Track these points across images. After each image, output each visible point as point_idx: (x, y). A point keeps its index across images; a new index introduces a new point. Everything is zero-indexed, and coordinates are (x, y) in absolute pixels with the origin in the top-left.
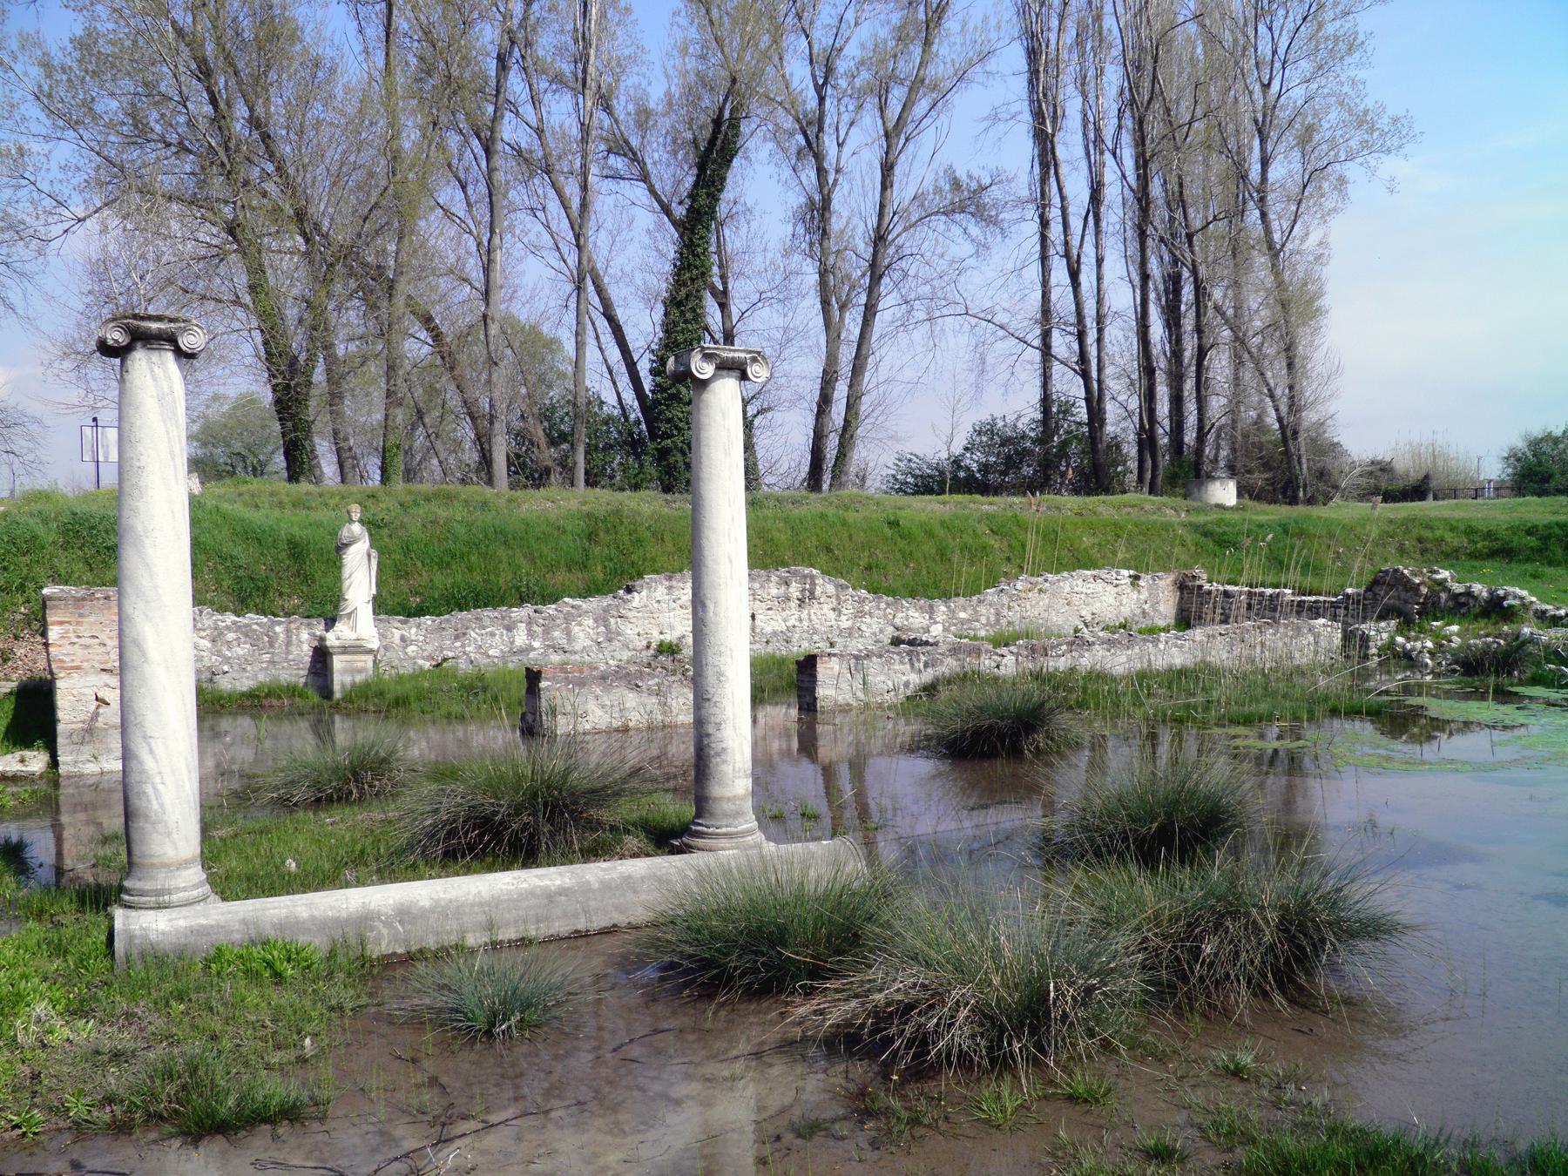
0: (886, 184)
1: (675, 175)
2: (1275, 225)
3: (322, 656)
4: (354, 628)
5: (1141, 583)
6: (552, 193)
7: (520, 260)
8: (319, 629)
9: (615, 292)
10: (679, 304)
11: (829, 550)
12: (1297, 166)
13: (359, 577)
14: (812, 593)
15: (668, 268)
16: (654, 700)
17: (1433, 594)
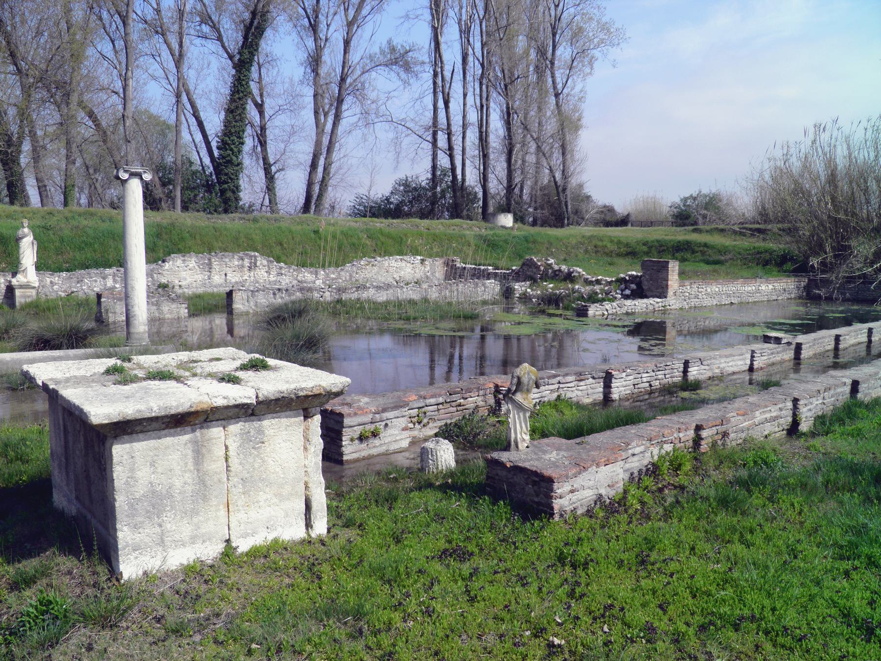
0: (346, 51)
1: (233, 37)
2: (558, 80)
4: (26, 277)
5: (426, 263)
6: (164, 47)
7: (145, 84)
8: (9, 278)
9: (200, 104)
10: (232, 112)
11: (281, 244)
12: (569, 50)
13: (28, 254)
14: (255, 264)
15: (228, 92)
16: (155, 308)
17: (546, 270)
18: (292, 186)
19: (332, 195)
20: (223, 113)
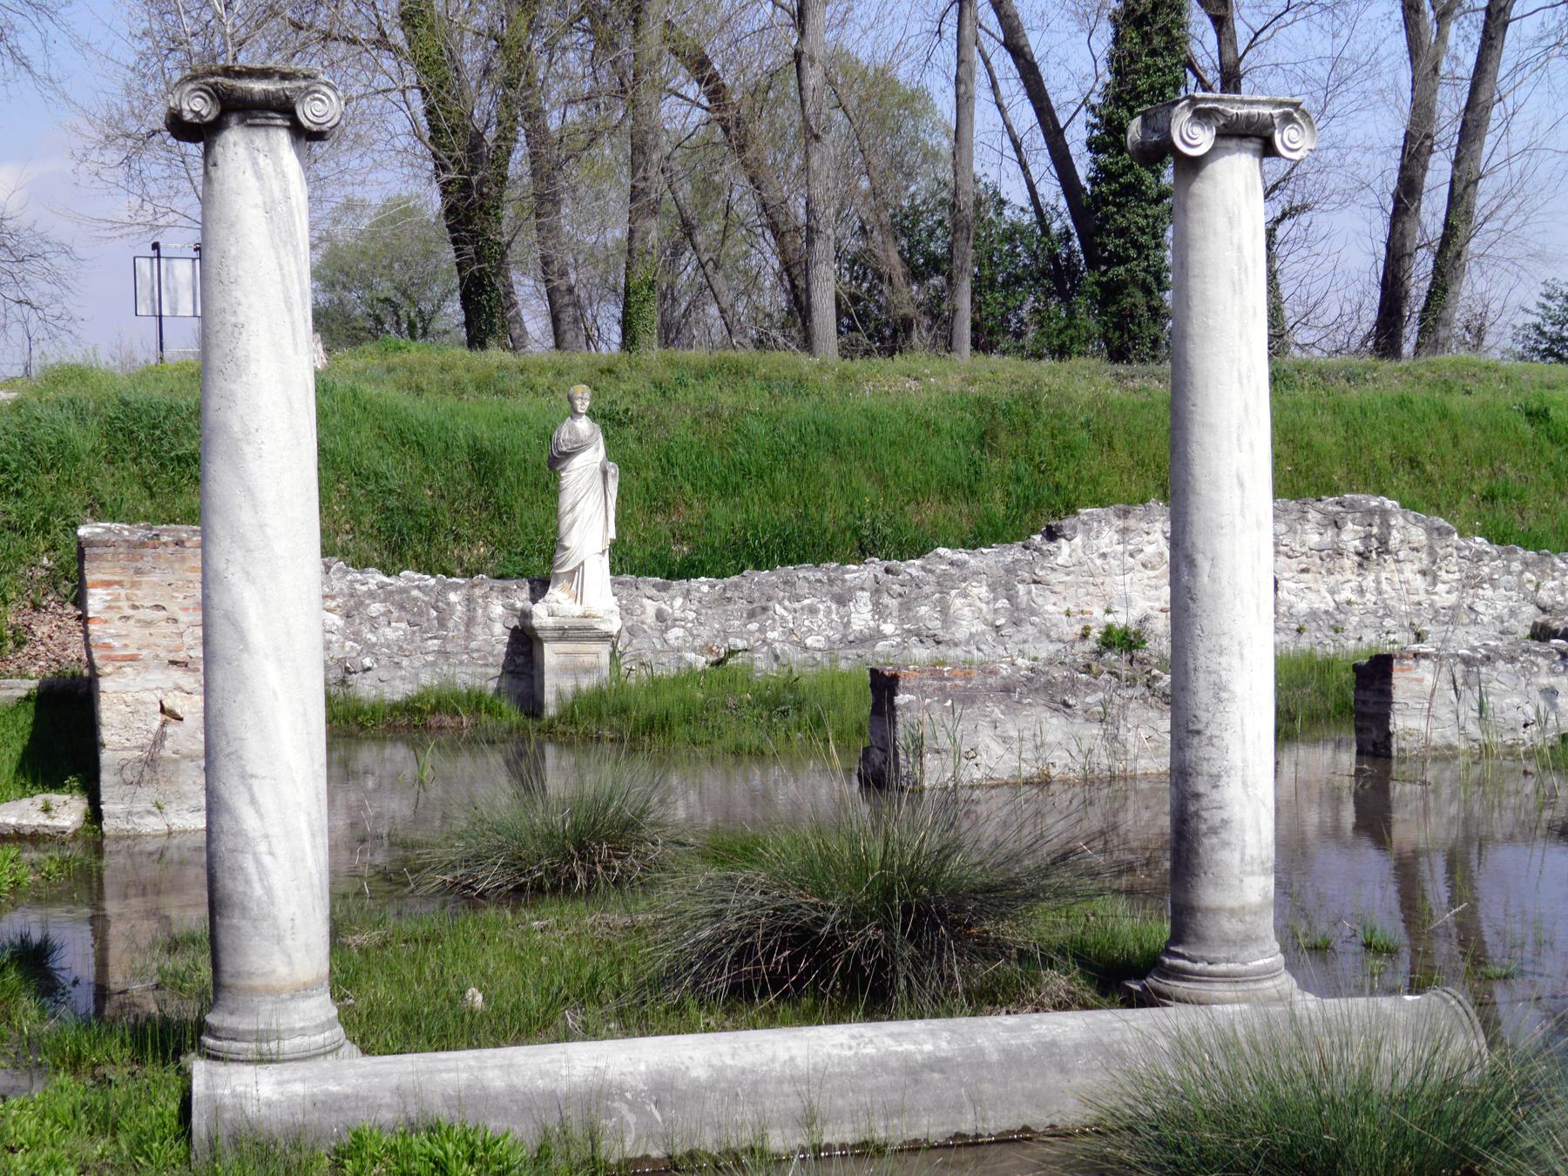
3: (525, 642)
8: (521, 599)
11: (1414, 463)
13: (588, 513)
14: (1383, 541)
16: (1096, 729)
19: (1481, 286)
20: (1105, 32)
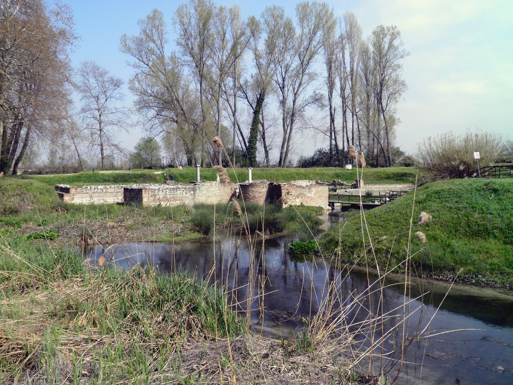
9: (241, 126)
18: (275, 156)
